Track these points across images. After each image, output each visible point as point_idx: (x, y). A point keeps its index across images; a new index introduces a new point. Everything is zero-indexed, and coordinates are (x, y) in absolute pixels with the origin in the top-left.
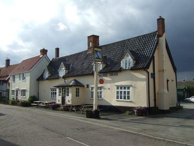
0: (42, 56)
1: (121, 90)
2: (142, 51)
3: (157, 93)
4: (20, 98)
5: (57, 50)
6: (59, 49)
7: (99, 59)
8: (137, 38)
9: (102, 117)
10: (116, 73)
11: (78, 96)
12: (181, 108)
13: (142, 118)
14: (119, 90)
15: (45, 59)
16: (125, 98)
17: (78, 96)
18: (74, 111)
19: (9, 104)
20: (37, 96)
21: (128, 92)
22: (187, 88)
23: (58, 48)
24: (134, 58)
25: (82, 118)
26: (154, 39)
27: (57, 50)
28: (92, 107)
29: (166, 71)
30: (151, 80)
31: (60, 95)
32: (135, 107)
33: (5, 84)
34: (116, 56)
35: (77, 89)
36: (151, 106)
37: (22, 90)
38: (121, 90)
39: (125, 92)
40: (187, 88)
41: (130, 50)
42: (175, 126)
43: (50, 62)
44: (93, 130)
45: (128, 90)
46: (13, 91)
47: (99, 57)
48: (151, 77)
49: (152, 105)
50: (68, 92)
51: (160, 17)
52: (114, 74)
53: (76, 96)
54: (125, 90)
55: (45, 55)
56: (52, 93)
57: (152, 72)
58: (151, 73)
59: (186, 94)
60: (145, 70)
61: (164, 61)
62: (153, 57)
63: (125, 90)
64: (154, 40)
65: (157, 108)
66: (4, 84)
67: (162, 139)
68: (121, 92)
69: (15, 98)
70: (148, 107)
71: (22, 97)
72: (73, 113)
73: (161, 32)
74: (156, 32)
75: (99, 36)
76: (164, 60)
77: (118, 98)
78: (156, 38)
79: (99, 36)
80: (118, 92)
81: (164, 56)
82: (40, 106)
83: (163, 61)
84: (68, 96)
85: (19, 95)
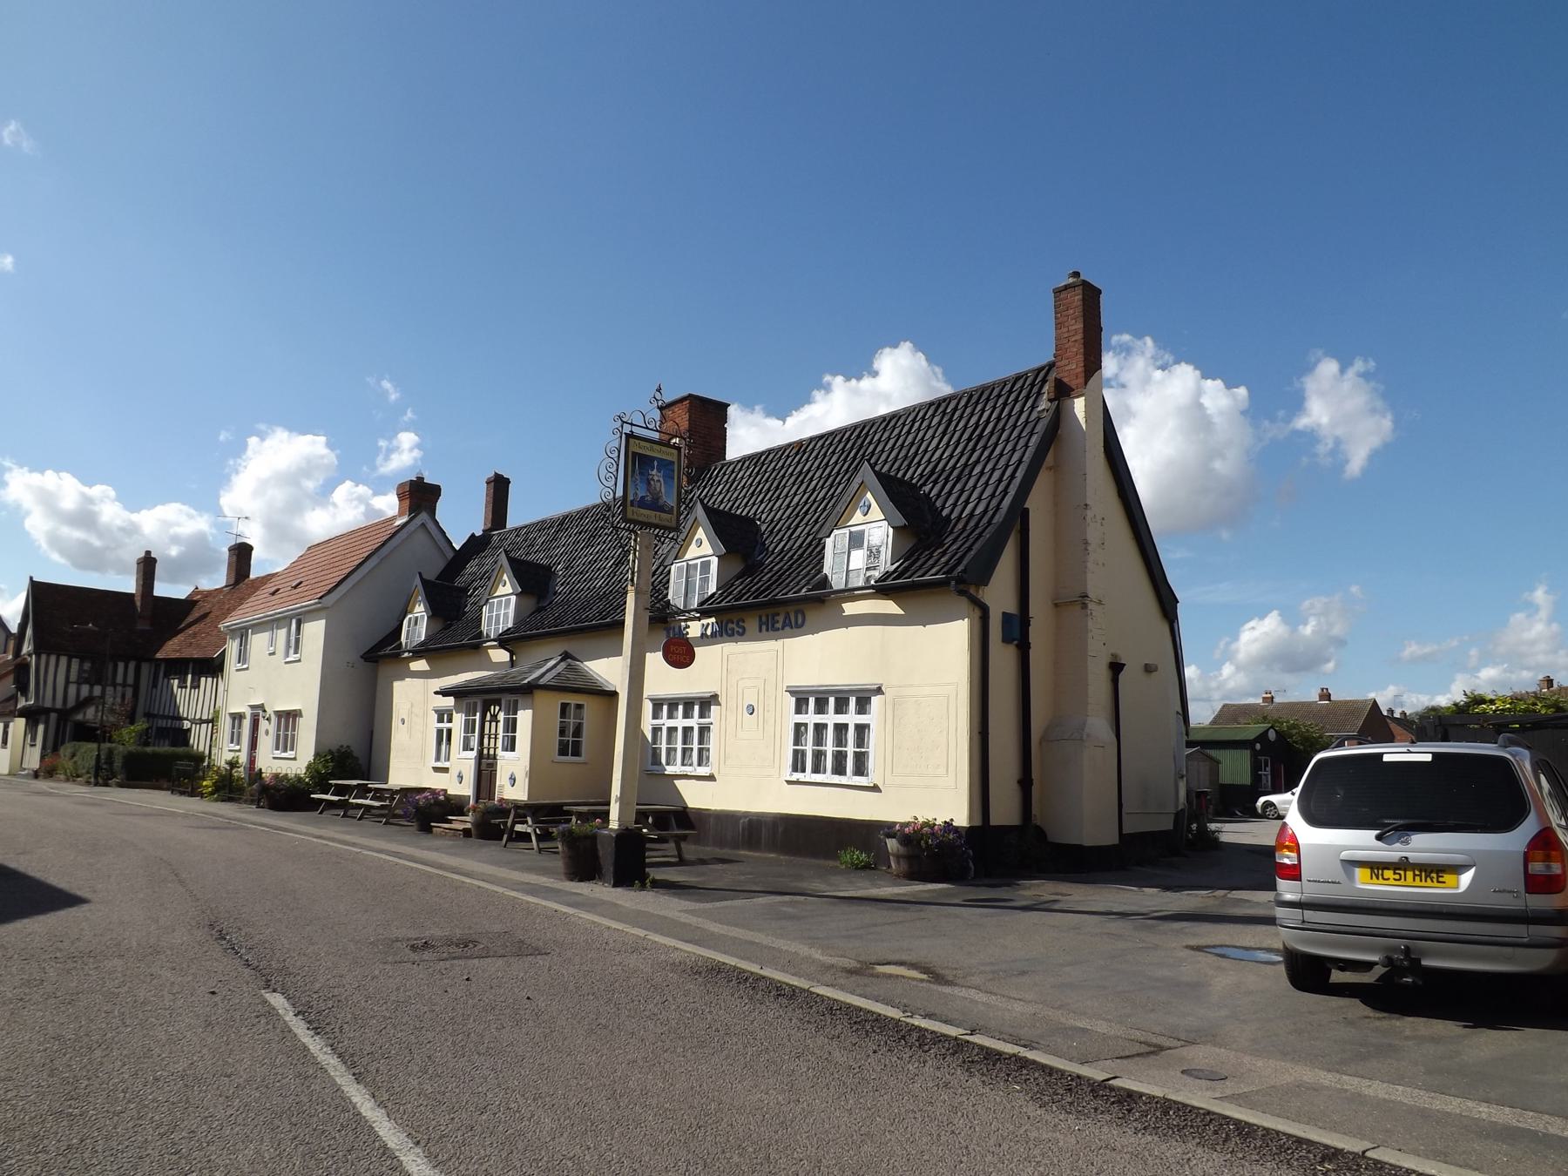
0: (405, 519)
1: (820, 719)
2: (959, 478)
3: (1044, 739)
4: (270, 762)
5: (499, 488)
6: (507, 482)
7: (661, 509)
8: (936, 411)
9: (656, 874)
11: (576, 753)
12: (1211, 843)
13: (949, 889)
14: (811, 718)
15: (421, 536)
16: (839, 769)
17: (576, 753)
18: (525, 837)
19: (201, 795)
20: (357, 751)
21: (862, 729)
22: (1272, 735)
24: (901, 521)
25: (544, 881)
26: (1033, 407)
27: (499, 488)
28: (605, 816)
29: (1100, 603)
30: (1003, 658)
31: (467, 747)
32: (891, 825)
33: (210, 679)
35: (564, 707)
36: (995, 820)
37: (279, 714)
38: (820, 719)
39: (841, 729)
40: (1272, 735)
43: (450, 555)
44: (523, 950)
45: (862, 719)
46: (237, 718)
47: (656, 498)
48: (1006, 639)
49: (1005, 812)
51: (1076, 274)
52: (781, 619)
54: (841, 719)
55: (423, 517)
56: (440, 732)
57: (1011, 607)
58: (1004, 614)
59: (1266, 773)
60: (962, 593)
61: (1090, 538)
62: (1019, 516)
63: (841, 719)
64: (1034, 415)
65: (1041, 833)
66: (203, 679)
67: (952, 1031)
68: (820, 728)
69: (243, 758)
70: (978, 822)
71: (278, 753)
72: (518, 852)
73: (1072, 369)
74: (1051, 366)
76: (1093, 534)
77: (798, 764)
78: (1043, 404)
80: (799, 729)
81: (1089, 514)
82: (359, 806)
83: (1086, 543)
84: (513, 749)
85: (266, 743)
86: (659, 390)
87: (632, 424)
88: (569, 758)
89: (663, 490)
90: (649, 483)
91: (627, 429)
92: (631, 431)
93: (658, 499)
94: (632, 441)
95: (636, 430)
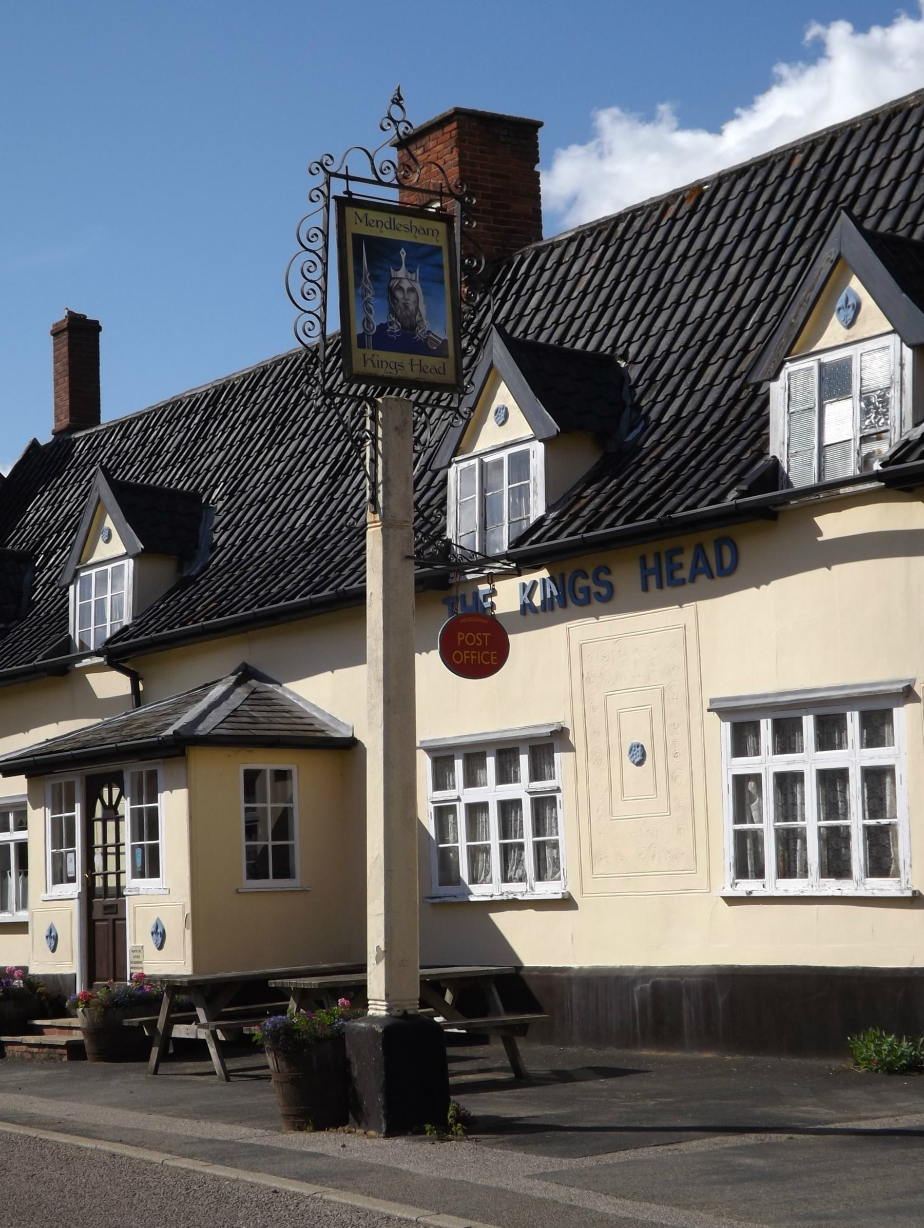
1: (786, 763)
10: (719, 544)
23: (97, 322)
25: (242, 1133)
31: (60, 876)
34: (723, 334)
38: (786, 763)
41: (871, 237)
42: (588, 792)
45: (876, 757)
50: (643, 1004)
52: (687, 559)
53: (256, 870)
54: (832, 759)
63: (832, 759)
75: (536, 125)
79: (536, 125)
84: (154, 872)
86: (397, 100)
87: (347, 178)
88: (270, 883)
89: (422, 307)
90: (391, 294)
91: (338, 187)
92: (348, 192)
93: (413, 328)
94: (350, 211)
95: (357, 189)
